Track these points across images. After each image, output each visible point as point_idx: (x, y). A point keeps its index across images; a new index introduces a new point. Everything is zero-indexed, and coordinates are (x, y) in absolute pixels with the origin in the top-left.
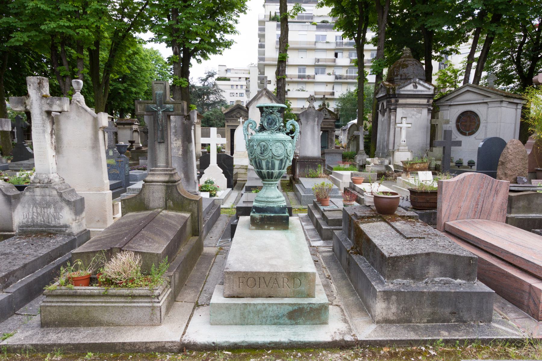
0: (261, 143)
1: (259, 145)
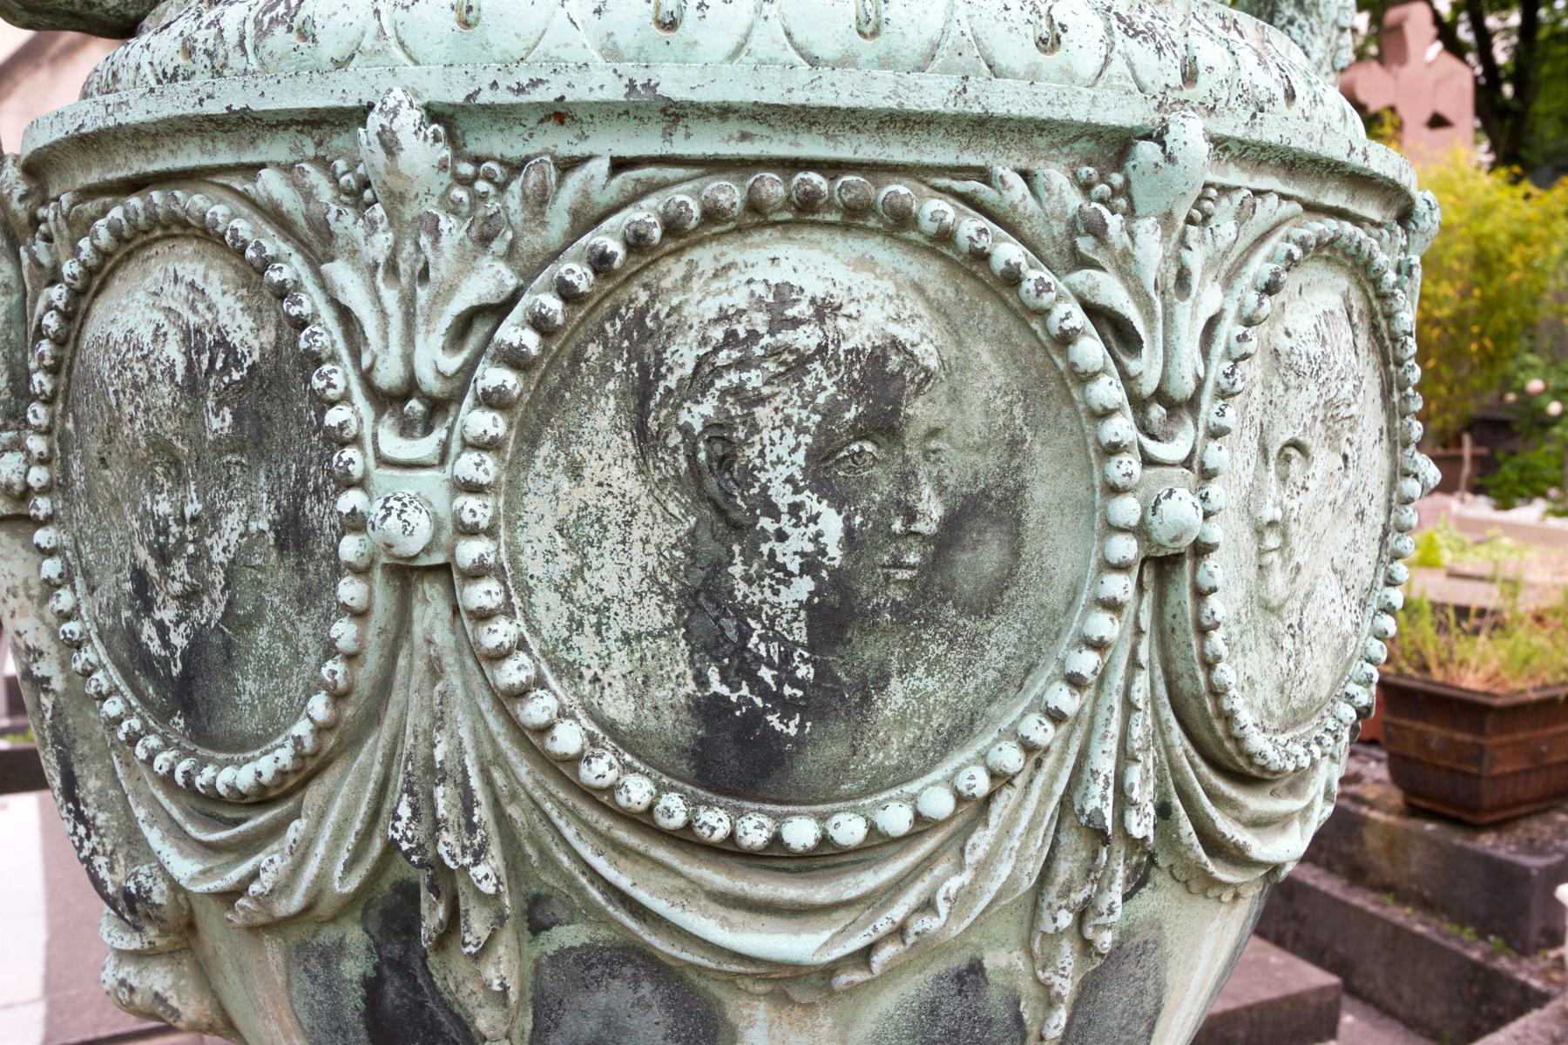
0: (714, 290)
1: (588, 350)
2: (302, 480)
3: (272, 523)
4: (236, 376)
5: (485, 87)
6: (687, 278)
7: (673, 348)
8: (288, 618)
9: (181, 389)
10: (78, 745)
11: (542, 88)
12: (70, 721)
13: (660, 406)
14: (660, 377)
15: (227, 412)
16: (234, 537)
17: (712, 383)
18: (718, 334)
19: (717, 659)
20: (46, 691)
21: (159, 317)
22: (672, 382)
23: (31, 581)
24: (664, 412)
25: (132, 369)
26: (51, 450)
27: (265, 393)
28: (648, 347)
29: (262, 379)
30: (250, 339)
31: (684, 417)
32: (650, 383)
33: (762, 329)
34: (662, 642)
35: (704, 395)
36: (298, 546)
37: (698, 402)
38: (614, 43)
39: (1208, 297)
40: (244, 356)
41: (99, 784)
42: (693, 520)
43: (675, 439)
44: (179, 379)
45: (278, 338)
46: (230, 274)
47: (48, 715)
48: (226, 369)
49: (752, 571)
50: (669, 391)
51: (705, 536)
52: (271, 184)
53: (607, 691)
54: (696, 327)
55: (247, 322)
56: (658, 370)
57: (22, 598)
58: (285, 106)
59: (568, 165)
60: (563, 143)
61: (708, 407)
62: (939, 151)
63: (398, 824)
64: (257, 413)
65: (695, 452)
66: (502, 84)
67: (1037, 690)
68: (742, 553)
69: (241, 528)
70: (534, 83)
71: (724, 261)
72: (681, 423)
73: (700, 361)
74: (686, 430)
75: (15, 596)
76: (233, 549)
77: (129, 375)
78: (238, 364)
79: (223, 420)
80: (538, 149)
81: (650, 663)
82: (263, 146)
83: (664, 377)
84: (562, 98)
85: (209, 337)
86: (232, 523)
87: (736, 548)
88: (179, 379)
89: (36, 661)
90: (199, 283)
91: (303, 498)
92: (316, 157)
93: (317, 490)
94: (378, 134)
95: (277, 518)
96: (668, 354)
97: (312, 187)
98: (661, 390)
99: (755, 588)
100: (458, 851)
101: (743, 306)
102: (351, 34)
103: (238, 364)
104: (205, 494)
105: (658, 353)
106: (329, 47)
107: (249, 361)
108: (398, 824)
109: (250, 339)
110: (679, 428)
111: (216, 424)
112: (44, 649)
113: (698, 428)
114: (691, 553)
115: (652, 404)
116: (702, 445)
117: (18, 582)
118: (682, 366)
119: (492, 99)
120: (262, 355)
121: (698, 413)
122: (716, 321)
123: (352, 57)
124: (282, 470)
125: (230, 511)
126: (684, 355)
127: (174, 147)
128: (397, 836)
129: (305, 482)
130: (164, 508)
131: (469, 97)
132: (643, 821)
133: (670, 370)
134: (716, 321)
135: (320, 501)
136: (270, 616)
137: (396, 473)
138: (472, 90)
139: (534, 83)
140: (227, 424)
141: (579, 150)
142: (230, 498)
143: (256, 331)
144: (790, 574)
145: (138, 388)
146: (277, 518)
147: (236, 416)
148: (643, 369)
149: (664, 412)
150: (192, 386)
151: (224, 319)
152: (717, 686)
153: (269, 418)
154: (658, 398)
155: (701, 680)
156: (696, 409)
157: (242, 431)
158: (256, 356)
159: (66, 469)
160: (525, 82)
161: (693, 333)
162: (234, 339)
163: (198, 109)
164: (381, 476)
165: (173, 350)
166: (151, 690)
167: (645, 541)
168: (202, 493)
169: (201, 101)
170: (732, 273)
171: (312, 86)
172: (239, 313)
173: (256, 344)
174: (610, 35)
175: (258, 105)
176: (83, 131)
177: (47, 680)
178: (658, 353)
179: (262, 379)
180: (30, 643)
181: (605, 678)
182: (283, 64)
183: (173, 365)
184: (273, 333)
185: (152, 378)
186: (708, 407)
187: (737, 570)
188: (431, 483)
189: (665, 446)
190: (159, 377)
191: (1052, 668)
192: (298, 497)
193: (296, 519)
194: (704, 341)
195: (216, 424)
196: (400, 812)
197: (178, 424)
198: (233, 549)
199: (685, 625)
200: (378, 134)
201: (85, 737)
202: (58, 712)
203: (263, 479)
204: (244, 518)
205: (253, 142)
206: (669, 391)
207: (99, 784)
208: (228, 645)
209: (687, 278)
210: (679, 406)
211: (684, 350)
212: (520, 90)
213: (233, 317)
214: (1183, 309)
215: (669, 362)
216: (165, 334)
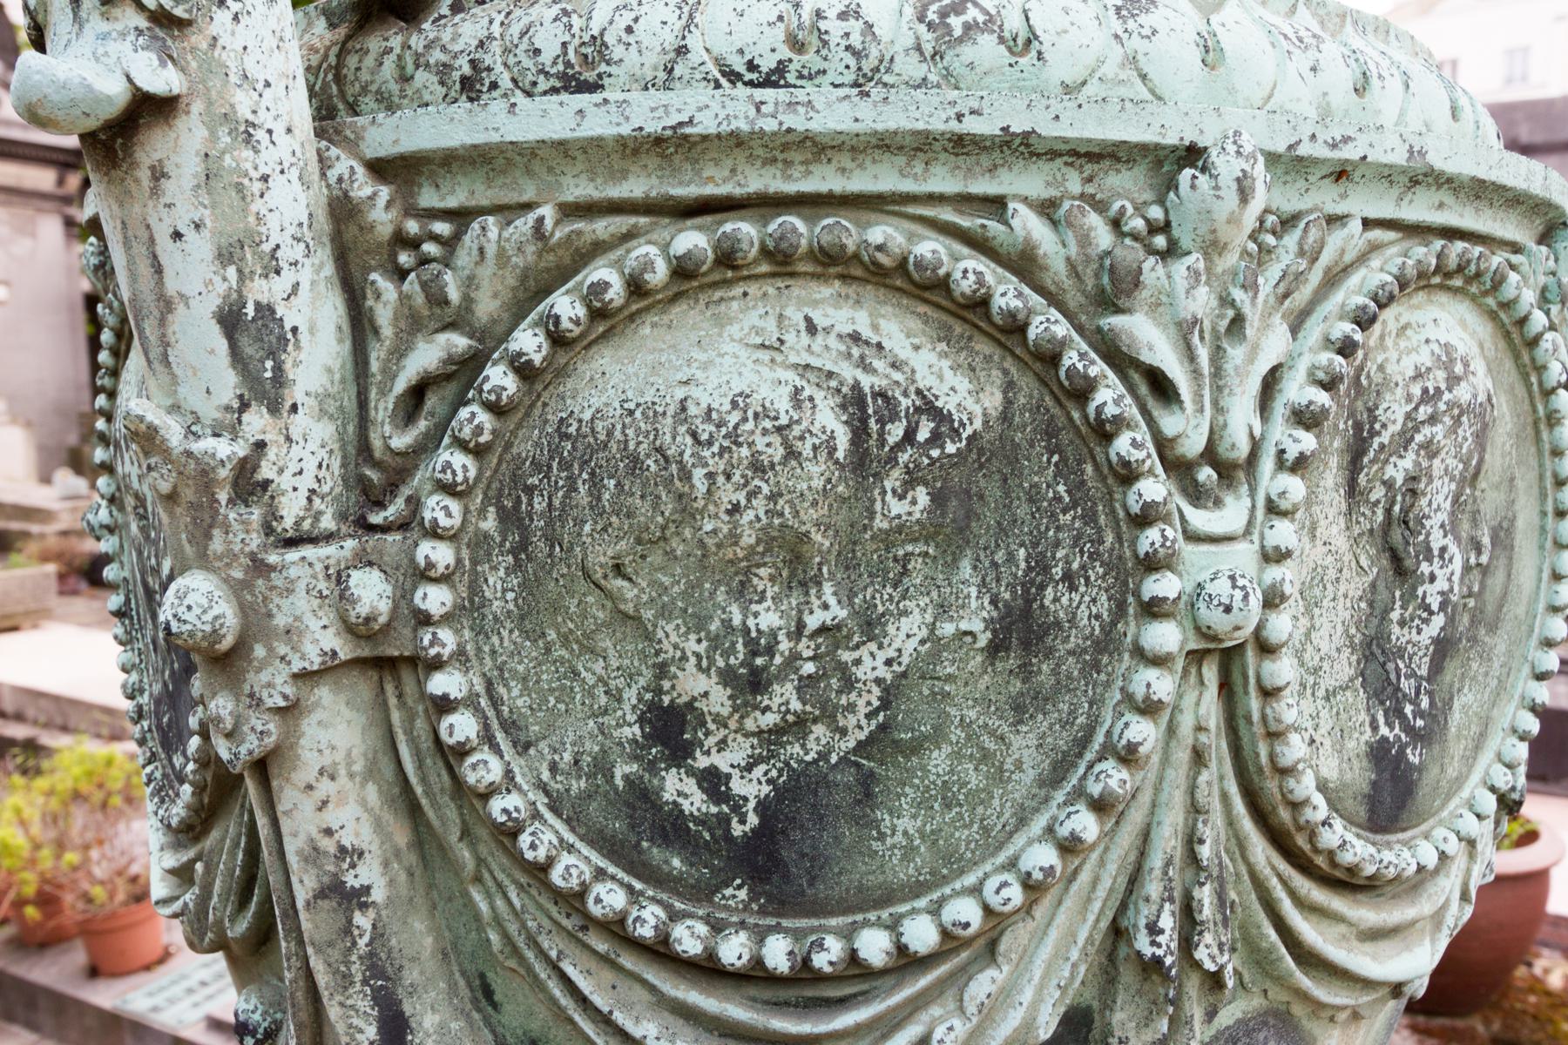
2: (1041, 565)
3: (988, 623)
4: (951, 448)
5: (1306, 139)
6: (1382, 337)
7: (1385, 405)
8: (992, 733)
9: (842, 467)
10: (405, 973)
11: (1351, 145)
12: (394, 942)
13: (1372, 462)
14: (1374, 433)
15: (922, 496)
16: (913, 643)
17: (1412, 438)
18: (1416, 391)
19: (1382, 703)
20: (364, 906)
21: (791, 377)
22: (1385, 438)
23: (355, 752)
24: (1375, 468)
25: (751, 445)
26: (459, 561)
27: (981, 467)
28: (1360, 405)
29: (981, 451)
30: (970, 403)
31: (1390, 471)
32: (1364, 440)
33: (1443, 386)
34: (1348, 693)
35: (1406, 449)
36: (1026, 645)
37: (1401, 457)
38: (1328, 104)
39: (1273, 343)
40: (962, 424)
41: (437, 1018)
42: (1375, 570)
43: (1378, 493)
44: (840, 455)
45: (1008, 403)
46: (915, 324)
47: (362, 942)
48: (936, 439)
49: (1407, 615)
50: (1382, 446)
51: (1381, 586)
52: (1027, 224)
53: (1321, 751)
54: (1401, 384)
55: (963, 384)
56: (1372, 427)
57: (343, 779)
58: (1087, 134)
59: (1334, 220)
60: (1327, 198)
61: (1407, 462)
62: (1511, 227)
63: (1160, 939)
64: (967, 492)
65: (1393, 503)
66: (1320, 138)
67: (1519, 690)
68: (1402, 596)
69: (924, 632)
70: (1346, 140)
71: (1403, 321)
72: (1386, 477)
73: (1408, 416)
74: (1389, 484)
75: (333, 778)
76: (905, 660)
77: (745, 451)
78: (955, 434)
79: (914, 502)
80: (1309, 206)
81: (1343, 716)
82: (1003, 173)
83: (1379, 434)
84: (1365, 157)
85: (905, 403)
86: (907, 633)
87: (1398, 594)
88: (840, 455)
89: (353, 866)
90: (866, 333)
91: (1042, 587)
92: (1082, 195)
93: (1068, 577)
94: (1238, 180)
95: (995, 614)
96: (1381, 408)
97: (1091, 229)
98: (1375, 446)
99: (1406, 630)
100: (1215, 951)
101: (1429, 364)
102: (1089, 58)
103: (955, 434)
104: (852, 595)
105: (1370, 411)
106: (1060, 68)
107: (969, 431)
108: (1160, 939)
109: (970, 403)
110: (1384, 483)
111: (897, 507)
112: (365, 846)
113: (1399, 482)
114: (1371, 604)
115: (1366, 460)
116: (1399, 498)
117: (339, 756)
118: (1394, 422)
119: (1311, 152)
120: (986, 423)
121: (1398, 469)
122: (1414, 378)
123: (1084, 83)
124: (1000, 556)
125: (906, 613)
126: (1394, 411)
127: (849, 164)
128: (1159, 952)
129: (1046, 569)
130: (768, 618)
131: (1291, 147)
132: (616, 928)
133: (1384, 426)
134: (1414, 378)
135: (1073, 588)
136: (957, 734)
137: (1212, 548)
138: (1293, 140)
139: (1346, 140)
140: (920, 507)
141: (1340, 209)
142: (904, 598)
143: (977, 393)
144: (1431, 613)
145: (758, 467)
146: (995, 614)
147: (938, 499)
148: (1358, 427)
149: (1375, 468)
150: (864, 462)
151: (925, 380)
152: (1384, 730)
153: (981, 497)
154: (1372, 454)
155: (1375, 728)
156: (1401, 463)
157: (943, 515)
158: (978, 424)
159: (474, 589)
160: (1338, 138)
161: (1399, 391)
162: (947, 403)
163: (954, 126)
164: (1189, 551)
165: (829, 419)
166: (676, 862)
167: (1346, 596)
168: (847, 595)
169: (960, 117)
170: (1409, 332)
171: (1124, 116)
172: (948, 374)
173: (978, 410)
174: (1325, 94)
175: (1048, 129)
176: (688, 130)
177: (367, 890)
178: (1370, 411)
179: (981, 451)
180: (347, 843)
181: (1318, 738)
182: (988, 80)
183: (832, 438)
184: (999, 397)
185: (792, 454)
186: (1407, 462)
187: (1395, 615)
188: (1243, 556)
189: (1367, 501)
190: (807, 451)
191: (1526, 670)
192: (1031, 589)
193: (1026, 613)
194: (1409, 399)
195: (897, 507)
196: (1161, 924)
197: (825, 511)
198: (905, 660)
199: (1362, 674)
200: (1238, 180)
201: (413, 960)
202: (378, 933)
203: (969, 570)
204: (929, 618)
205: (993, 169)
206: (1382, 446)
207: (437, 1018)
208: (867, 781)
209: (1382, 337)
210: (1386, 461)
211: (1395, 407)
212: (1334, 146)
213: (941, 377)
214: (1236, 354)
215: (1383, 418)
216: (811, 399)
